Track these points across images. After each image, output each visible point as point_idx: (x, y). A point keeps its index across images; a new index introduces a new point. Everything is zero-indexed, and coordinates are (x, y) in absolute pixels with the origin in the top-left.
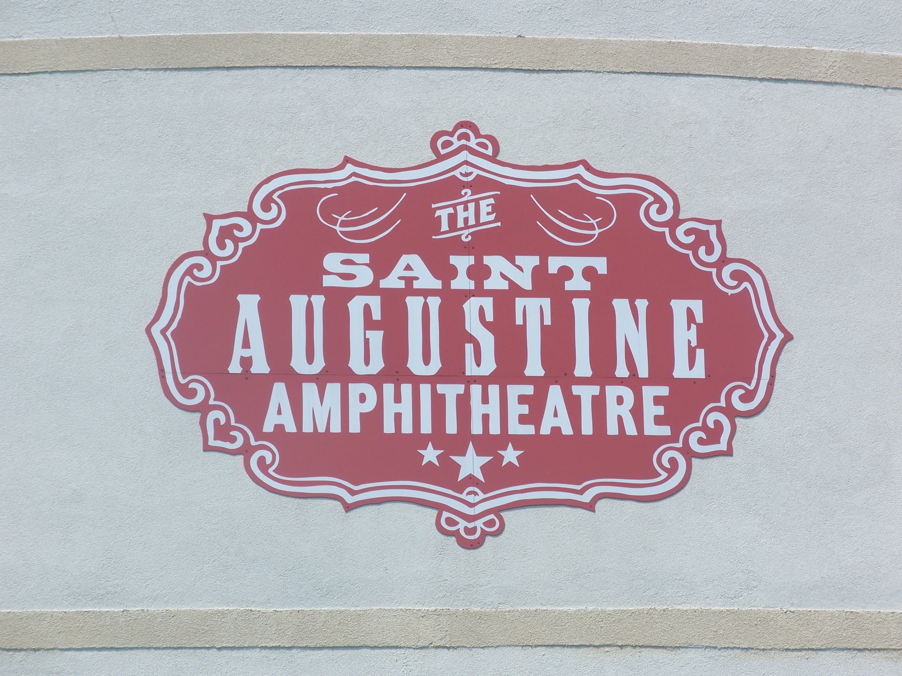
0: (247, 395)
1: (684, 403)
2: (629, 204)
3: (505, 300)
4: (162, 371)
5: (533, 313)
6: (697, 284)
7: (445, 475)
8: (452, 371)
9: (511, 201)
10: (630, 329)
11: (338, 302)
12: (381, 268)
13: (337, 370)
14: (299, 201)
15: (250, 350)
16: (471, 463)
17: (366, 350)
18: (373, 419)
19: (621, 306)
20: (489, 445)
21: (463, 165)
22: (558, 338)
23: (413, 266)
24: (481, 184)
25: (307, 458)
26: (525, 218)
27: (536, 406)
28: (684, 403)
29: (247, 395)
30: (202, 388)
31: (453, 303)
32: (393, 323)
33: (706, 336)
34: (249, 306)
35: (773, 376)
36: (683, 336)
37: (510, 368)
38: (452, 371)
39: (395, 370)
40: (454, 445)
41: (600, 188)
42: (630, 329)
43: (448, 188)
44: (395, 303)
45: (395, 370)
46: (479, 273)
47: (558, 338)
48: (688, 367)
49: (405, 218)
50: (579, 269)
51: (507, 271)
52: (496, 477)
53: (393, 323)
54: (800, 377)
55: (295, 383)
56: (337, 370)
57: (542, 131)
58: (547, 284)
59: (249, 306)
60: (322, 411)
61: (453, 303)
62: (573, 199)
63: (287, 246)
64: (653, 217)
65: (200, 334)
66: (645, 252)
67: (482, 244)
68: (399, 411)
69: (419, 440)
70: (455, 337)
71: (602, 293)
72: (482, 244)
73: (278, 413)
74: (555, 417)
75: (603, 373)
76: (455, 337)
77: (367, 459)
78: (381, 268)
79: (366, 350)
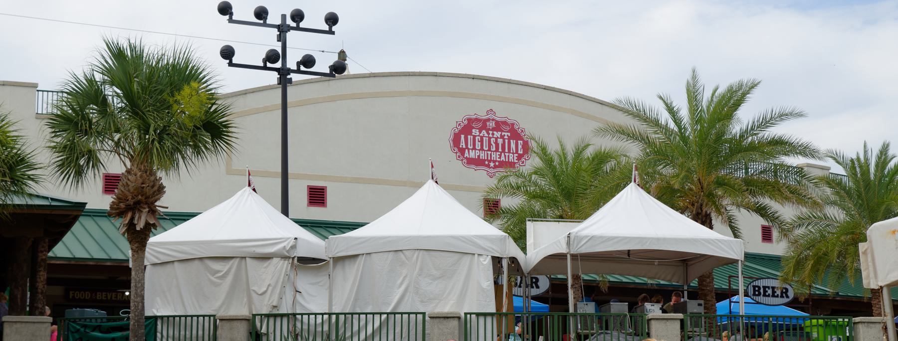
0: (462, 151)
1: (520, 157)
2: (513, 125)
3: (496, 139)
4: (453, 95)
5: (500, 141)
6: (522, 139)
8: (489, 150)
9: (497, 123)
10: (513, 146)
11: (474, 137)
12: (480, 132)
13: (474, 148)
14: (469, 120)
16: (492, 164)
17: (478, 146)
18: (479, 156)
20: (494, 162)
21: (491, 116)
23: (484, 132)
24: (493, 120)
26: (499, 126)
27: (500, 155)
28: (520, 157)
29: (462, 151)
30: (456, 149)
31: (490, 138)
32: (482, 141)
33: (523, 147)
34: (463, 136)
36: (520, 147)
37: (497, 150)
38: (489, 150)
39: (482, 149)
40: (490, 161)
41: (509, 122)
42: (513, 146)
43: (489, 120)
44: (482, 138)
45: (482, 149)
46: (493, 134)
49: (483, 124)
51: (497, 134)
52: (495, 167)
53: (482, 141)
55: (469, 150)
56: (474, 148)
57: (503, 112)
58: (502, 137)
59: (463, 136)
60: (472, 154)
61: (490, 138)
62: (505, 123)
63: (467, 127)
64: (516, 127)
65: (456, 141)
66: (516, 135)
68: (483, 155)
69: (485, 160)
71: (509, 139)
72: (493, 130)
73: (466, 155)
74: (503, 158)
75: (509, 152)
77: (477, 162)
78: (480, 132)
79: (478, 146)
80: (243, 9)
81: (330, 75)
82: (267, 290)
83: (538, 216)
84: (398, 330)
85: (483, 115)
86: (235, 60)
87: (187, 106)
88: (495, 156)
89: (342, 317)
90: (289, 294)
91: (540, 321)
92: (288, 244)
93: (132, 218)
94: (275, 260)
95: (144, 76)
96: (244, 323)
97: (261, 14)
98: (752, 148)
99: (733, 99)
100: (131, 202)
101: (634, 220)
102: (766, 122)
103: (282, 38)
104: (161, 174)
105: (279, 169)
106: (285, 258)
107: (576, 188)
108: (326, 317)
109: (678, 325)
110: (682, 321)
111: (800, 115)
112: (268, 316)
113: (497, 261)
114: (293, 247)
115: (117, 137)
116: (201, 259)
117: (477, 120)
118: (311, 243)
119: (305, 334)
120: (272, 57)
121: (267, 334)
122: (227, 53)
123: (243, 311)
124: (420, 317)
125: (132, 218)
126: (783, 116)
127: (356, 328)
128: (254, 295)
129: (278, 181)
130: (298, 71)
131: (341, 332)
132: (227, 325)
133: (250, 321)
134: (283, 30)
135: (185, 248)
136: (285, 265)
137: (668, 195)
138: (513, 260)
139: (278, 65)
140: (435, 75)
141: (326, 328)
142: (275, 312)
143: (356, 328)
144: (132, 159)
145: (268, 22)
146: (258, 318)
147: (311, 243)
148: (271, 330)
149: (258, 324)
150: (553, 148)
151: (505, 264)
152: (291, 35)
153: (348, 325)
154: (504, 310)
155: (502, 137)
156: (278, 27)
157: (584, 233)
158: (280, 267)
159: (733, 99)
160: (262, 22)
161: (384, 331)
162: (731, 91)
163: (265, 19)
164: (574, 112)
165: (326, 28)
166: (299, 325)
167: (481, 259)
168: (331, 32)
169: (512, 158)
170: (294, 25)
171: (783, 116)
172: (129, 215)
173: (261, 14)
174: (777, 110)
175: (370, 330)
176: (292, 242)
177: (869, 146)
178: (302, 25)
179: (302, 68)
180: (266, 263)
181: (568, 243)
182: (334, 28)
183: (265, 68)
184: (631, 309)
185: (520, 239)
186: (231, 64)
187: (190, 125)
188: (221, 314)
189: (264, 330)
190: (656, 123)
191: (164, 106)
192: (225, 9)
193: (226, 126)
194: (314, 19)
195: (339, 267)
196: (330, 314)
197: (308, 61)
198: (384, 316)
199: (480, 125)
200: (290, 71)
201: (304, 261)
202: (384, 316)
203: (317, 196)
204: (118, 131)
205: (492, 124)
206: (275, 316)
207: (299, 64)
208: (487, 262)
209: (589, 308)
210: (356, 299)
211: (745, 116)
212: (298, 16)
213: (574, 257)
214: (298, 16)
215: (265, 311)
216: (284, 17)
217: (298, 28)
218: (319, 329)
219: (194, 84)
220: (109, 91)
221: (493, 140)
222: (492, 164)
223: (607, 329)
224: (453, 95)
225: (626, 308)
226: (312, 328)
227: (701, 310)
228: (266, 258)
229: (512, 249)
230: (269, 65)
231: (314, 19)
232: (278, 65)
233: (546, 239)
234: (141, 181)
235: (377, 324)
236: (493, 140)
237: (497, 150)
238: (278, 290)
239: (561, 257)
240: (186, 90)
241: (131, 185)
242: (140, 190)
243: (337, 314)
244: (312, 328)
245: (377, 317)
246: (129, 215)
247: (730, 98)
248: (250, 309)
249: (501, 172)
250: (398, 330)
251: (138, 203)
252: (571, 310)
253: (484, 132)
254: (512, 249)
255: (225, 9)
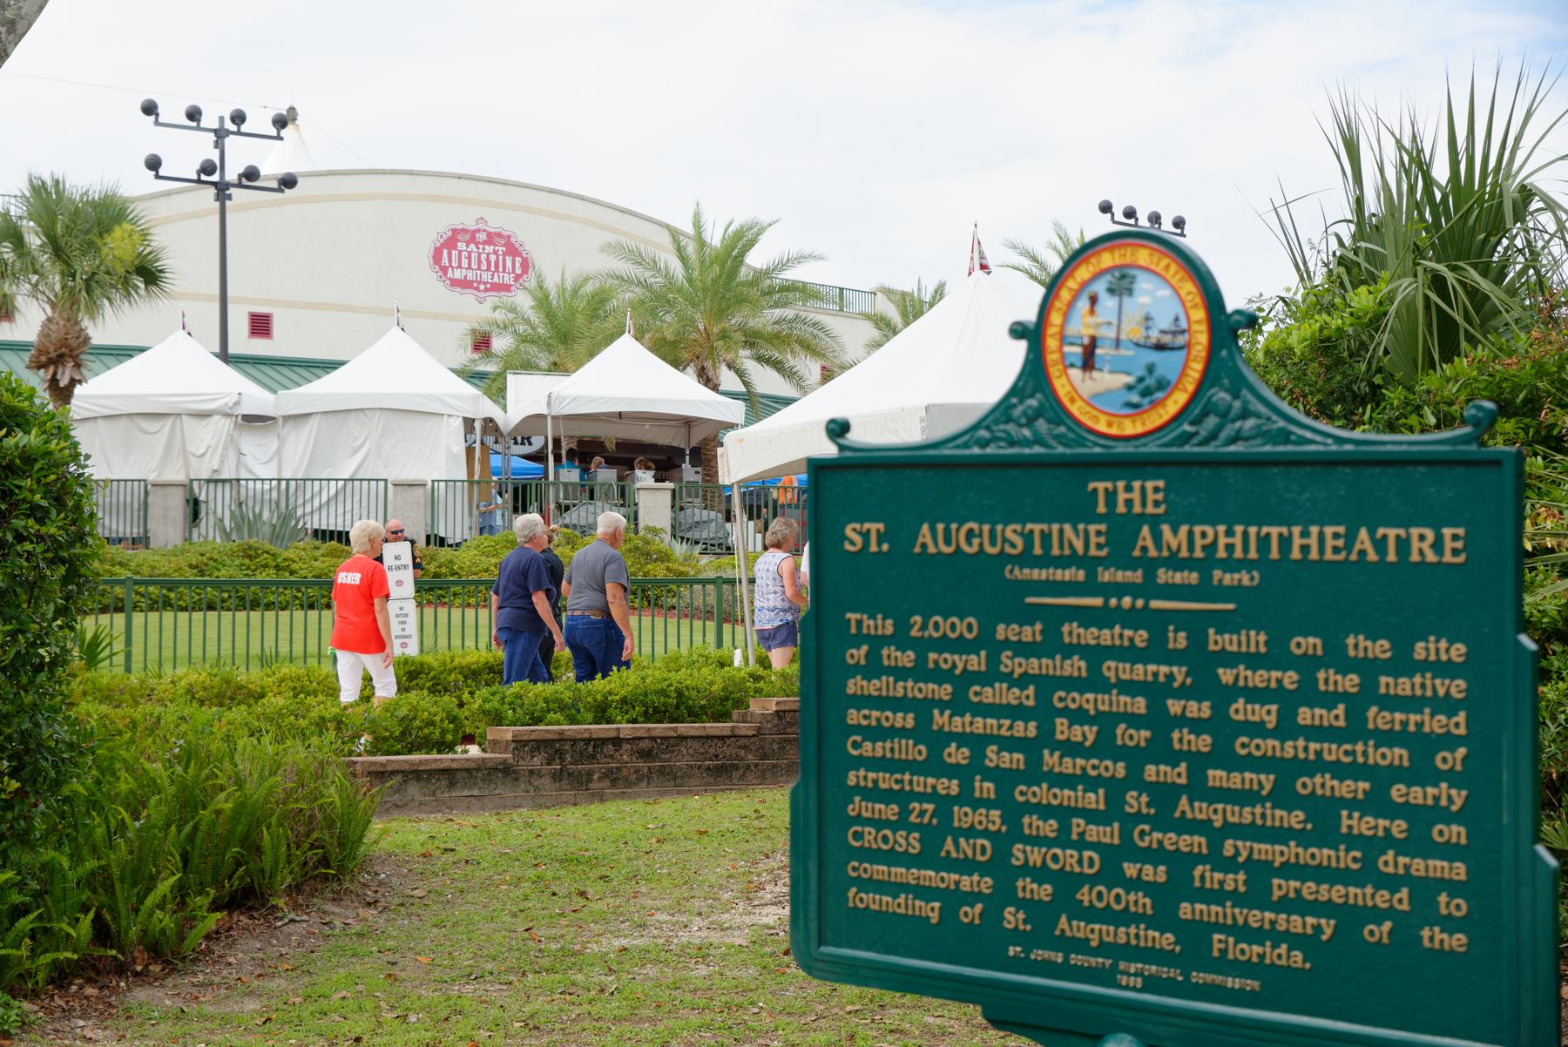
0: (444, 270)
1: (517, 278)
4: (434, 198)
5: (493, 258)
7: (477, 289)
9: (489, 234)
10: (509, 260)
13: (460, 267)
14: (455, 231)
15: (445, 261)
16: (482, 287)
17: (465, 263)
19: (1364, 785)
22: (497, 263)
23: (472, 246)
25: (455, 283)
26: (491, 238)
28: (517, 278)
29: (444, 270)
35: (369, 197)
37: (489, 269)
39: (470, 267)
42: (509, 260)
45: (470, 267)
47: (497, 263)
48: (518, 271)
50: (501, 249)
51: (489, 249)
52: (486, 290)
53: (469, 258)
54: (1152, 198)
56: (460, 267)
57: (496, 222)
58: (495, 252)
60: (458, 274)
62: (499, 235)
66: (512, 250)
67: (484, 243)
68: (471, 276)
70: (480, 262)
71: (505, 254)
72: (484, 243)
73: (450, 274)
74: (496, 280)
76: (480, 262)
77: (464, 284)
79: (465, 263)
80: (173, 111)
81: (279, 190)
82: (207, 452)
83: (528, 366)
84: (357, 498)
85: (471, 225)
86: (162, 172)
87: (118, 245)
88: (486, 277)
89: (293, 483)
90: (231, 460)
91: (524, 487)
92: (231, 400)
93: (55, 374)
94: (216, 418)
95: (267, 529)
96: (180, 489)
97: (194, 114)
98: (770, 292)
99: (742, 240)
100: (53, 355)
101: (628, 380)
102: (784, 265)
103: (219, 145)
104: (86, 323)
105: (216, 291)
106: (227, 415)
107: (568, 334)
108: (274, 483)
109: (668, 495)
110: (674, 491)
111: (820, 258)
112: (208, 481)
113: (469, 424)
114: (237, 404)
115: (35, 278)
116: (129, 415)
117: (464, 231)
118: (257, 398)
119: (250, 503)
120: (208, 168)
121: (206, 502)
122: (154, 164)
123: (178, 476)
124: (382, 484)
125: (55, 374)
126: (800, 259)
127: (308, 496)
128: (191, 458)
129: (216, 306)
130: (240, 185)
131: (292, 500)
132: (159, 491)
133: (187, 486)
134: (220, 134)
135: (110, 403)
136: (227, 424)
137: (672, 352)
138: (489, 423)
139: (215, 178)
140: (411, 173)
141: (274, 495)
142: (216, 477)
143: (308, 496)
144: (53, 306)
145: (203, 125)
146: (195, 484)
147: (257, 398)
148: (211, 497)
149: (196, 490)
150: (551, 283)
151: (478, 425)
152: (229, 141)
153: (300, 493)
154: (476, 478)
155: (495, 252)
156: (215, 131)
157: (566, 393)
158: (222, 426)
159: (742, 240)
160: (194, 124)
161: (341, 498)
162: (739, 234)
163: (198, 121)
164: (586, 222)
165: (274, 132)
166: (243, 491)
167: (452, 420)
168: (279, 138)
169: (508, 279)
170: (234, 128)
171: (800, 259)
172: (52, 369)
173: (194, 114)
174: (794, 253)
175: (324, 499)
176: (235, 398)
177: (923, 285)
178: (244, 128)
179: (245, 182)
180: (205, 422)
181: (549, 404)
182: (283, 133)
183: (199, 181)
184: (620, 478)
185: (498, 393)
186: (157, 177)
187: (121, 271)
188: (152, 477)
189: (202, 497)
190: (654, 265)
191: (90, 247)
192: (150, 109)
193: (161, 271)
194: (259, 121)
195: (289, 426)
196: (279, 480)
197: (251, 174)
198: (341, 483)
199: (467, 237)
200: (229, 185)
201: (250, 419)
202: (341, 483)
203: (260, 325)
204: (36, 272)
205: (482, 237)
206: (216, 481)
207: (240, 176)
208: (458, 424)
209: (571, 475)
210: (310, 463)
211: (757, 259)
212: (238, 118)
213: (554, 418)
214: (238, 118)
215: (205, 476)
216: (222, 119)
217: (239, 133)
218: (267, 497)
219: (126, 226)
220: (28, 226)
221: (483, 257)
222: (482, 287)
223: (592, 498)
224: (434, 198)
225: (615, 476)
226: (259, 497)
227: (699, 478)
228: (205, 415)
229: (488, 408)
230: (204, 177)
231: (259, 121)
232: (215, 178)
233: (530, 395)
234: (63, 331)
235: (333, 492)
236: (483, 257)
237: (489, 269)
238: (219, 452)
239: (542, 417)
240: (118, 232)
241: (54, 336)
242: (64, 342)
243: (288, 480)
244: (259, 497)
245: (333, 483)
246: (52, 369)
247: (740, 238)
248: (187, 474)
249: (492, 299)
250: (357, 498)
251: (61, 356)
252: (551, 478)
253: (472, 246)
254: (488, 408)
255: (150, 109)
